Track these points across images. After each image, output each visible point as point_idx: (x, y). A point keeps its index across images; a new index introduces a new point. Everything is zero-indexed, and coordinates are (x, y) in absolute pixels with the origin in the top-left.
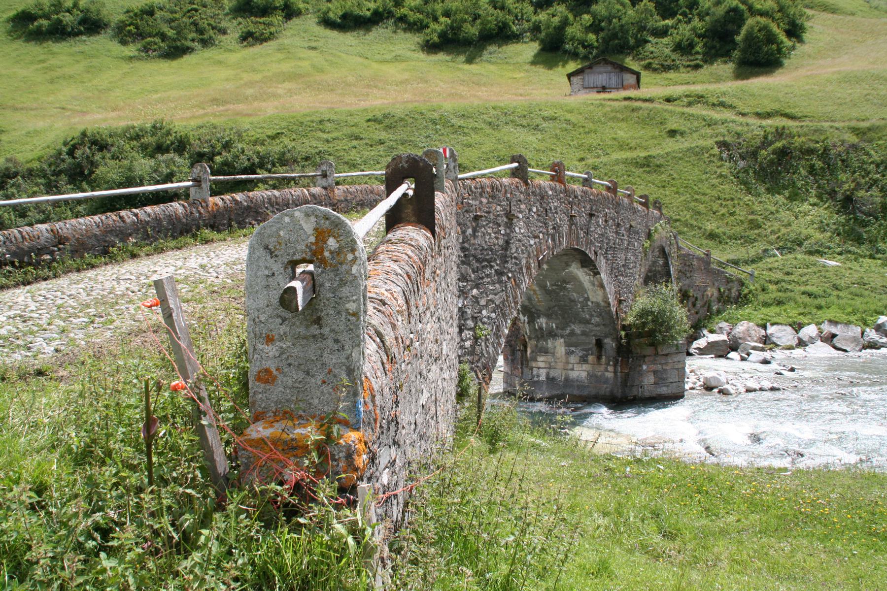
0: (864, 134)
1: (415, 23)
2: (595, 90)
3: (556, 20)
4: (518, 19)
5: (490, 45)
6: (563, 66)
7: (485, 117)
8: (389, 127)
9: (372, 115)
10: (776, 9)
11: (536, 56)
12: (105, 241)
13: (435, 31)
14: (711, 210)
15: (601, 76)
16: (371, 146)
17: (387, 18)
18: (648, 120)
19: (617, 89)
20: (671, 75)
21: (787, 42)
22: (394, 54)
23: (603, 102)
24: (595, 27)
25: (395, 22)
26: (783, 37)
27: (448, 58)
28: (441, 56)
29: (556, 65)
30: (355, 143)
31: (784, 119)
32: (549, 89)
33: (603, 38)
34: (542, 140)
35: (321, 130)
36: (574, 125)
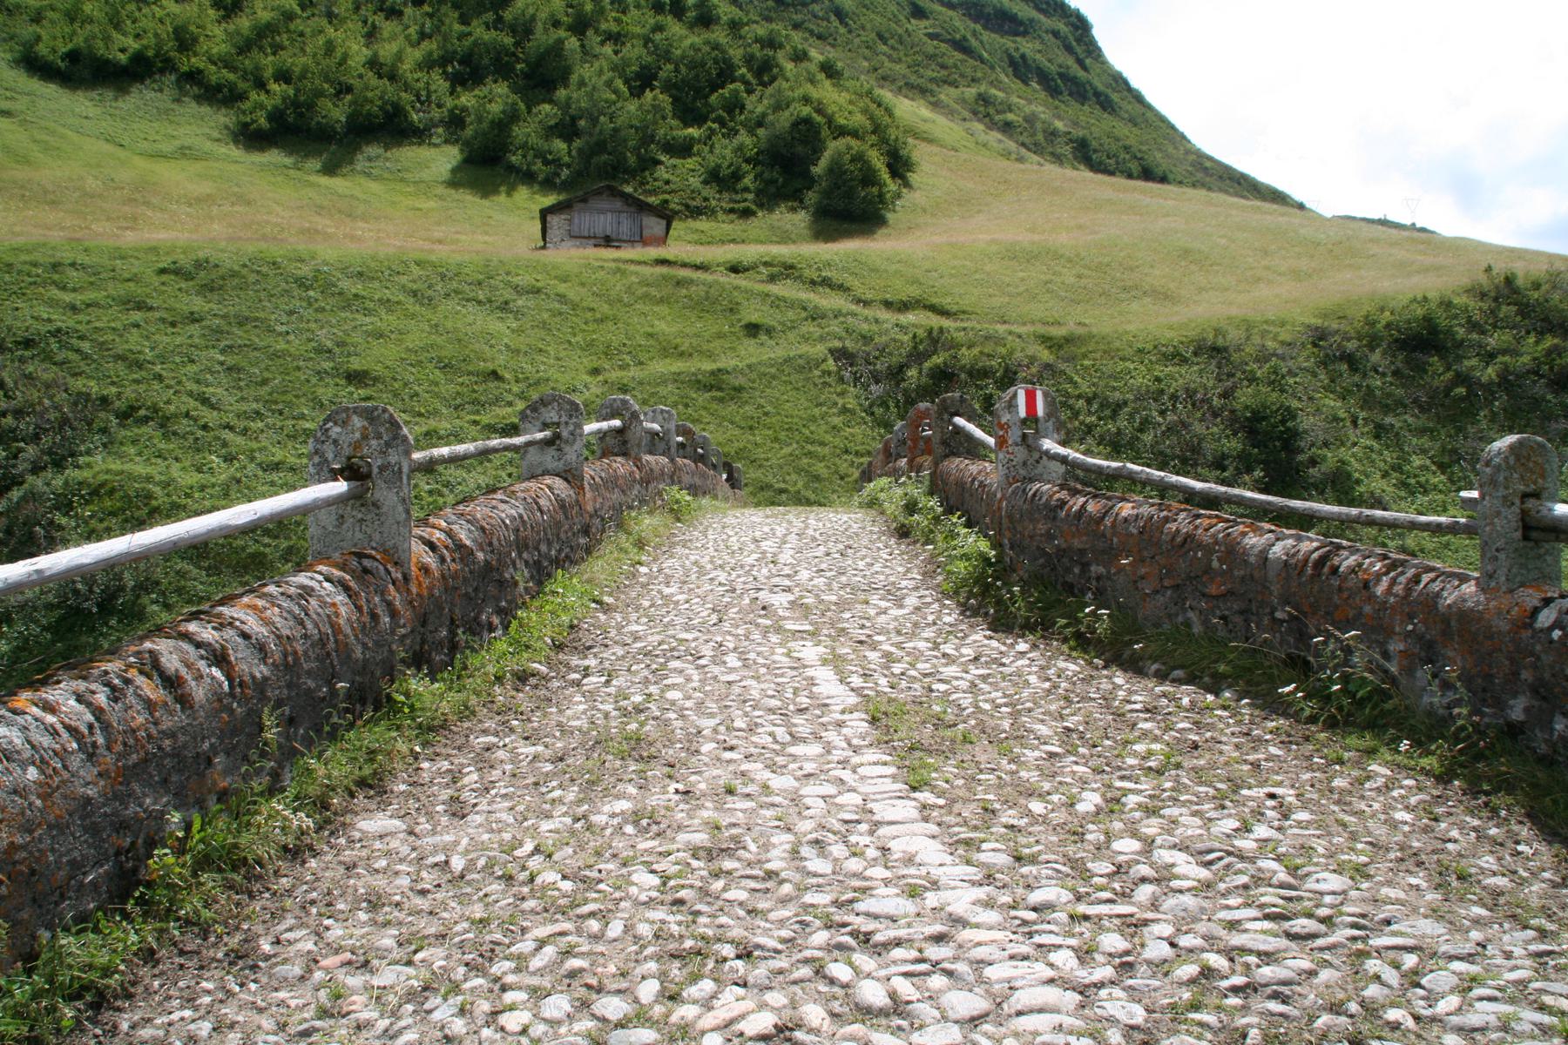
0: (1060, 347)
1: (219, 88)
2: (592, 241)
3: (495, 108)
4: (423, 100)
5: (368, 143)
6: (509, 194)
7: (404, 279)
8: (208, 288)
9: (170, 260)
10: (869, 128)
11: (454, 171)
12: (122, 826)
13: (262, 106)
14: (836, 472)
15: (602, 219)
16: (173, 325)
17: (162, 71)
18: (707, 304)
19: (632, 242)
20: (703, 224)
21: (892, 186)
22: (177, 143)
23: (622, 266)
24: (567, 129)
25: (178, 81)
26: (885, 175)
27: (288, 161)
28: (274, 156)
29: (496, 192)
30: (137, 316)
31: (930, 314)
32: (486, 233)
33: (580, 150)
34: (519, 331)
35: (54, 283)
36: (575, 307)
